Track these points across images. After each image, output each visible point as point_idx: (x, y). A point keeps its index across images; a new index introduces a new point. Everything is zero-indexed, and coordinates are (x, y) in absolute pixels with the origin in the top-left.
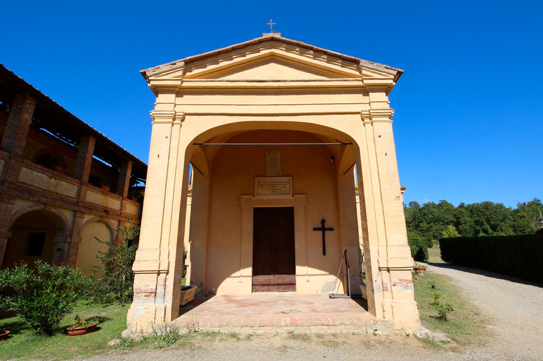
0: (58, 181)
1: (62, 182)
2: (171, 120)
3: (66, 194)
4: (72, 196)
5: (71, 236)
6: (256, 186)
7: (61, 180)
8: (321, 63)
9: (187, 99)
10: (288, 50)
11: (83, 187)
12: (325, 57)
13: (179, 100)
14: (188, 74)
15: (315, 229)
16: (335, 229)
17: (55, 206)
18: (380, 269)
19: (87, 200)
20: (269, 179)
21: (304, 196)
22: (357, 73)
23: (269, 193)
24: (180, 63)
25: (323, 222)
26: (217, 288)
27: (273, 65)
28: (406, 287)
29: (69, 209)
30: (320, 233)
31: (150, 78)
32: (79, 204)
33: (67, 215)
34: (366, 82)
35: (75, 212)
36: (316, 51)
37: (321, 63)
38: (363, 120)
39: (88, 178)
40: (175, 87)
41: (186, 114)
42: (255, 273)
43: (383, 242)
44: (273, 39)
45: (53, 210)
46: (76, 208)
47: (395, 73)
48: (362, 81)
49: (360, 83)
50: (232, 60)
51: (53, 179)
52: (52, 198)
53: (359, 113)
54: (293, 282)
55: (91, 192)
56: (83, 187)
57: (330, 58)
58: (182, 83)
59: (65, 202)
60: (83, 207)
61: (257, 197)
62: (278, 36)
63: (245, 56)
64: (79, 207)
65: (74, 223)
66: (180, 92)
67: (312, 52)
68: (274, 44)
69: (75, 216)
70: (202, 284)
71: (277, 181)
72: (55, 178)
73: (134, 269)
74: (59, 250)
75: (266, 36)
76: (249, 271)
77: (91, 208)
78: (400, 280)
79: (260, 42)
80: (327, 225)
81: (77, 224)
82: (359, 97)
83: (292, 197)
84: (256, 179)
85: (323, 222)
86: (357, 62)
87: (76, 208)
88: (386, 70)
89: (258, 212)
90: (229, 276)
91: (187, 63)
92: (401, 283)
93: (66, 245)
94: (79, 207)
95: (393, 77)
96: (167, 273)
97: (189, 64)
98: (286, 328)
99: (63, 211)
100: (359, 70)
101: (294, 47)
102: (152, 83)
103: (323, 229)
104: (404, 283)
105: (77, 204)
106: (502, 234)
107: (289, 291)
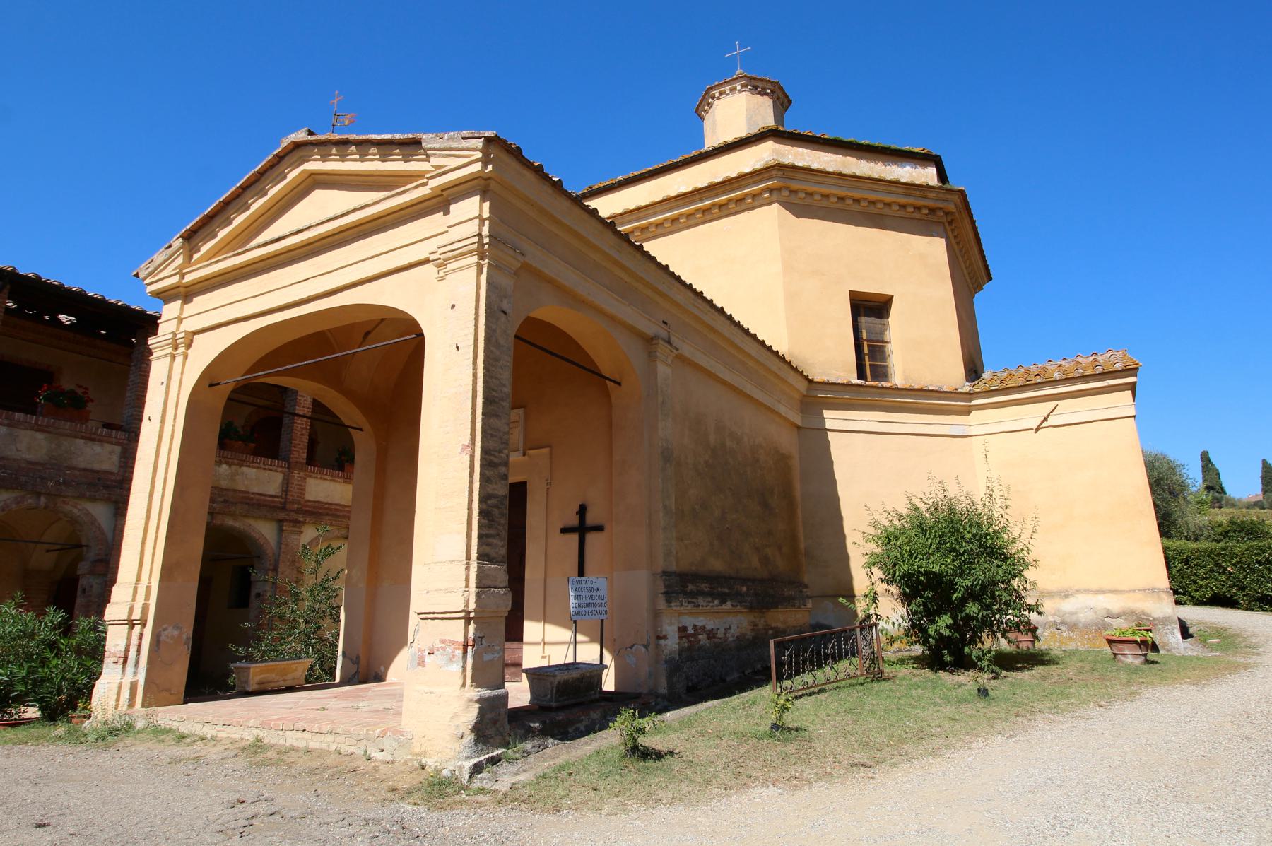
0: (234, 467)
1: (245, 469)
2: (170, 350)
3: (256, 490)
4: (272, 493)
5: (275, 570)
7: (241, 466)
8: (373, 165)
9: (200, 302)
11: (296, 474)
13: (190, 309)
14: (196, 256)
15: (564, 531)
16: (607, 527)
17: (234, 516)
19: (308, 497)
21: (547, 450)
24: (177, 243)
25: (582, 510)
26: (387, 668)
27: (318, 195)
28: (451, 659)
29: (265, 518)
30: (574, 538)
32: (288, 506)
33: (265, 530)
34: (435, 183)
35: (280, 522)
36: (359, 143)
37: (373, 165)
39: (305, 455)
40: (176, 287)
41: (195, 333)
44: (297, 146)
45: (230, 522)
46: (282, 515)
47: (479, 143)
50: (248, 208)
51: (224, 466)
52: (225, 501)
53: (426, 261)
55: (317, 481)
56: (296, 474)
58: (183, 276)
59: (257, 505)
60: (297, 511)
62: (301, 136)
63: (266, 194)
64: (290, 512)
65: (279, 543)
66: (186, 293)
69: (281, 531)
70: (358, 657)
72: (226, 463)
73: (107, 617)
74: (258, 595)
75: (285, 142)
77: (321, 512)
78: (443, 641)
79: (280, 158)
80: (591, 519)
81: (287, 545)
82: (435, 222)
83: (521, 458)
85: (582, 510)
86: (417, 143)
87: (282, 515)
88: (465, 144)
92: (444, 649)
93: (268, 587)
94: (290, 512)
95: (479, 155)
96: (144, 625)
97: (192, 237)
99: (252, 522)
102: (150, 289)
103: (582, 528)
104: (449, 650)
105: (283, 508)
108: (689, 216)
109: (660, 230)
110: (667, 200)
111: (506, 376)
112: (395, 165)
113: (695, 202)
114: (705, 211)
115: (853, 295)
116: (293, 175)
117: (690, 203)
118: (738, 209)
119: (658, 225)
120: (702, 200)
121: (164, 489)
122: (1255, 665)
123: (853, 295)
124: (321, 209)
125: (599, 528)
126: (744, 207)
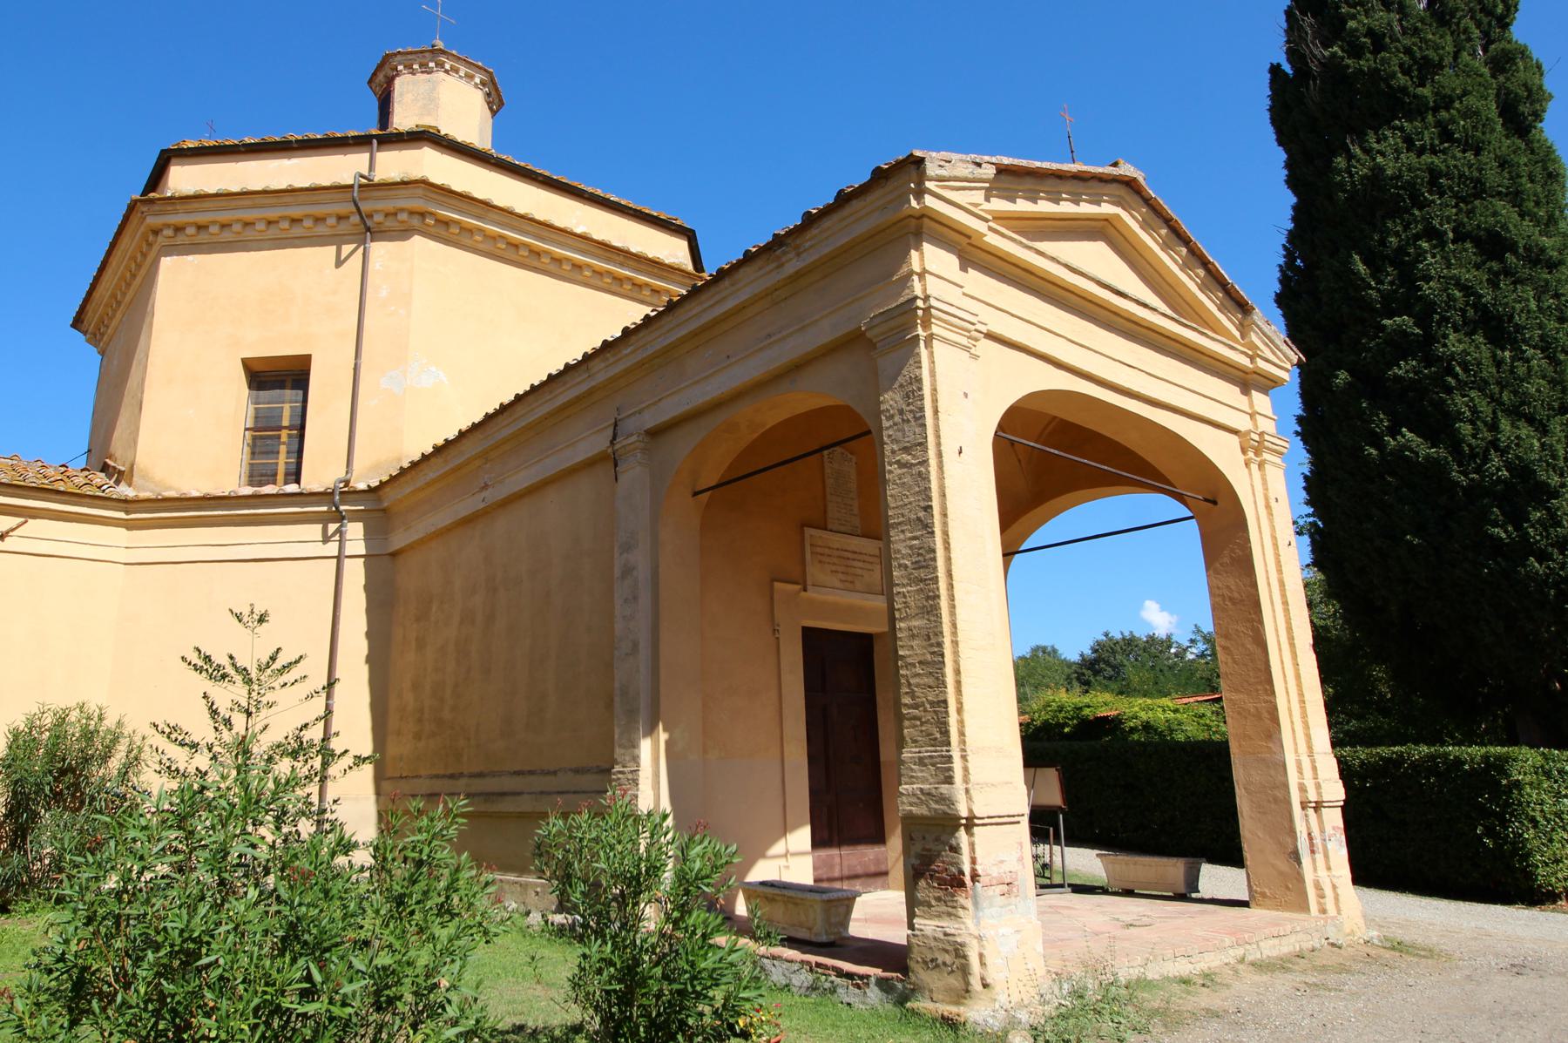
6: (808, 556)
9: (976, 281)
10: (1145, 225)
12: (1201, 272)
18: (1304, 806)
20: (837, 541)
22: (1237, 334)
23: (838, 584)
27: (1101, 247)
31: (929, 185)
37: (1190, 283)
38: (1244, 451)
42: (818, 842)
43: (1303, 748)
48: (1252, 359)
49: (1244, 361)
54: (883, 868)
57: (1210, 281)
61: (812, 594)
66: (972, 254)
67: (1184, 250)
68: (1128, 198)
71: (852, 548)
76: (802, 837)
84: (809, 531)
89: (814, 640)
90: (763, 856)
91: (1002, 170)
97: (1010, 179)
98: (1231, 952)
100: (1244, 329)
101: (1159, 222)
106: (355, 730)
107: (876, 889)
108: (599, 273)
109: (442, 231)
110: (584, 238)
111: (143, 338)
112: (1209, 303)
113: (614, 263)
114: (619, 280)
115: (247, 363)
116: (1107, 209)
117: (608, 260)
118: (614, 288)
119: (558, 261)
120: (622, 265)
121: (1298, 677)
122: (731, 1008)
123: (247, 363)
124: (1094, 261)
125: (337, 734)
126: (468, 242)
